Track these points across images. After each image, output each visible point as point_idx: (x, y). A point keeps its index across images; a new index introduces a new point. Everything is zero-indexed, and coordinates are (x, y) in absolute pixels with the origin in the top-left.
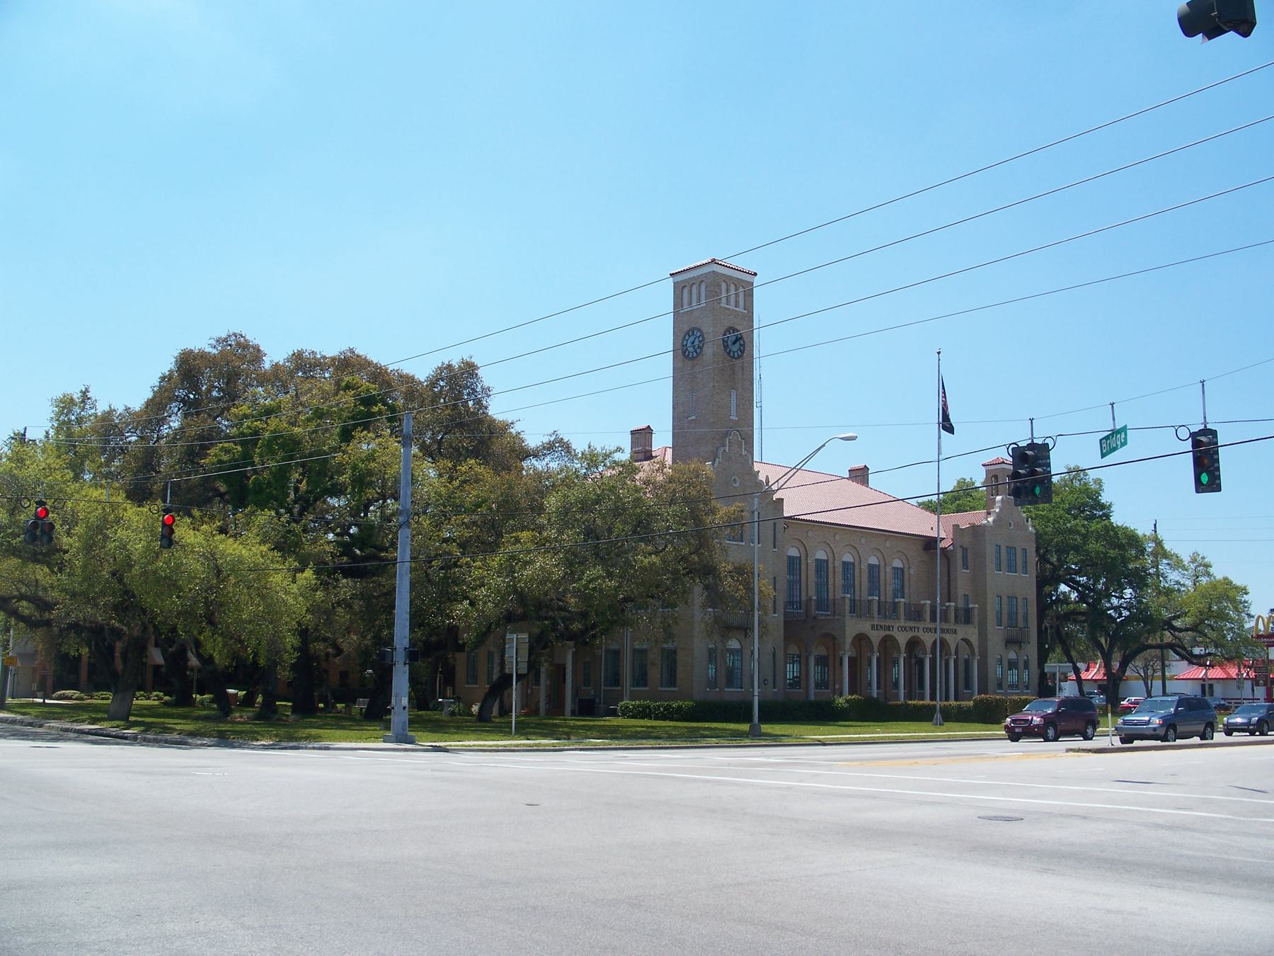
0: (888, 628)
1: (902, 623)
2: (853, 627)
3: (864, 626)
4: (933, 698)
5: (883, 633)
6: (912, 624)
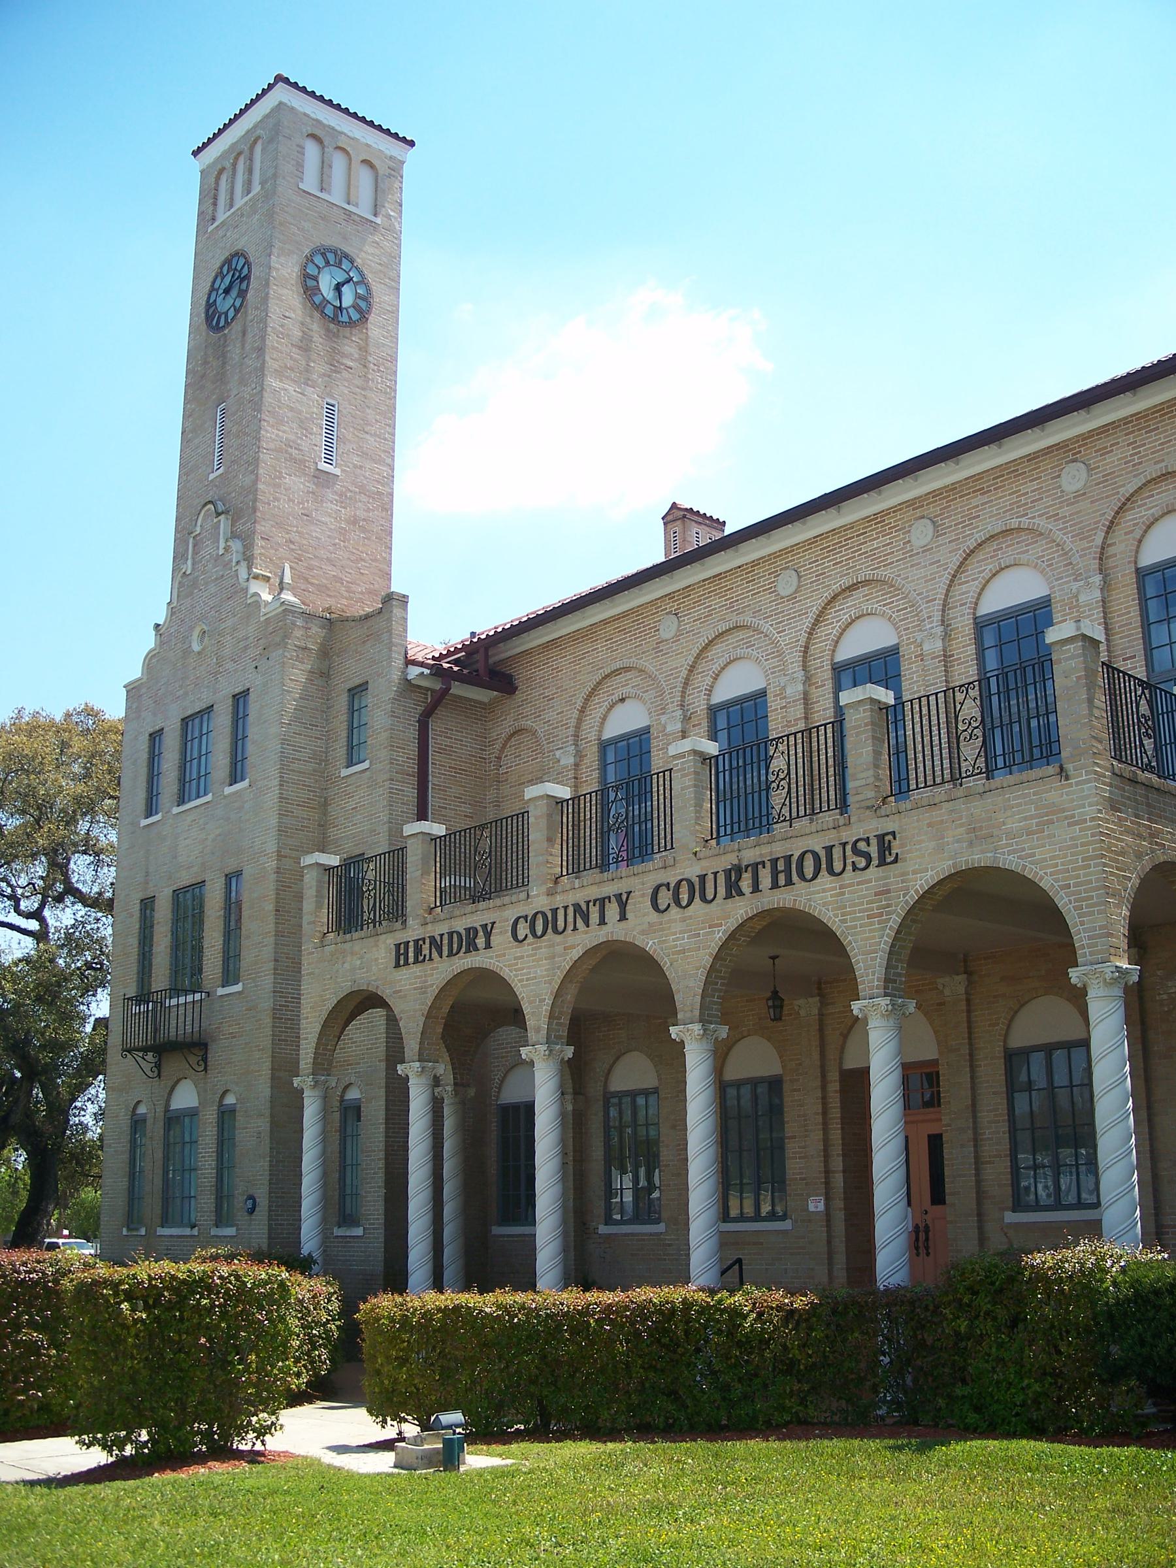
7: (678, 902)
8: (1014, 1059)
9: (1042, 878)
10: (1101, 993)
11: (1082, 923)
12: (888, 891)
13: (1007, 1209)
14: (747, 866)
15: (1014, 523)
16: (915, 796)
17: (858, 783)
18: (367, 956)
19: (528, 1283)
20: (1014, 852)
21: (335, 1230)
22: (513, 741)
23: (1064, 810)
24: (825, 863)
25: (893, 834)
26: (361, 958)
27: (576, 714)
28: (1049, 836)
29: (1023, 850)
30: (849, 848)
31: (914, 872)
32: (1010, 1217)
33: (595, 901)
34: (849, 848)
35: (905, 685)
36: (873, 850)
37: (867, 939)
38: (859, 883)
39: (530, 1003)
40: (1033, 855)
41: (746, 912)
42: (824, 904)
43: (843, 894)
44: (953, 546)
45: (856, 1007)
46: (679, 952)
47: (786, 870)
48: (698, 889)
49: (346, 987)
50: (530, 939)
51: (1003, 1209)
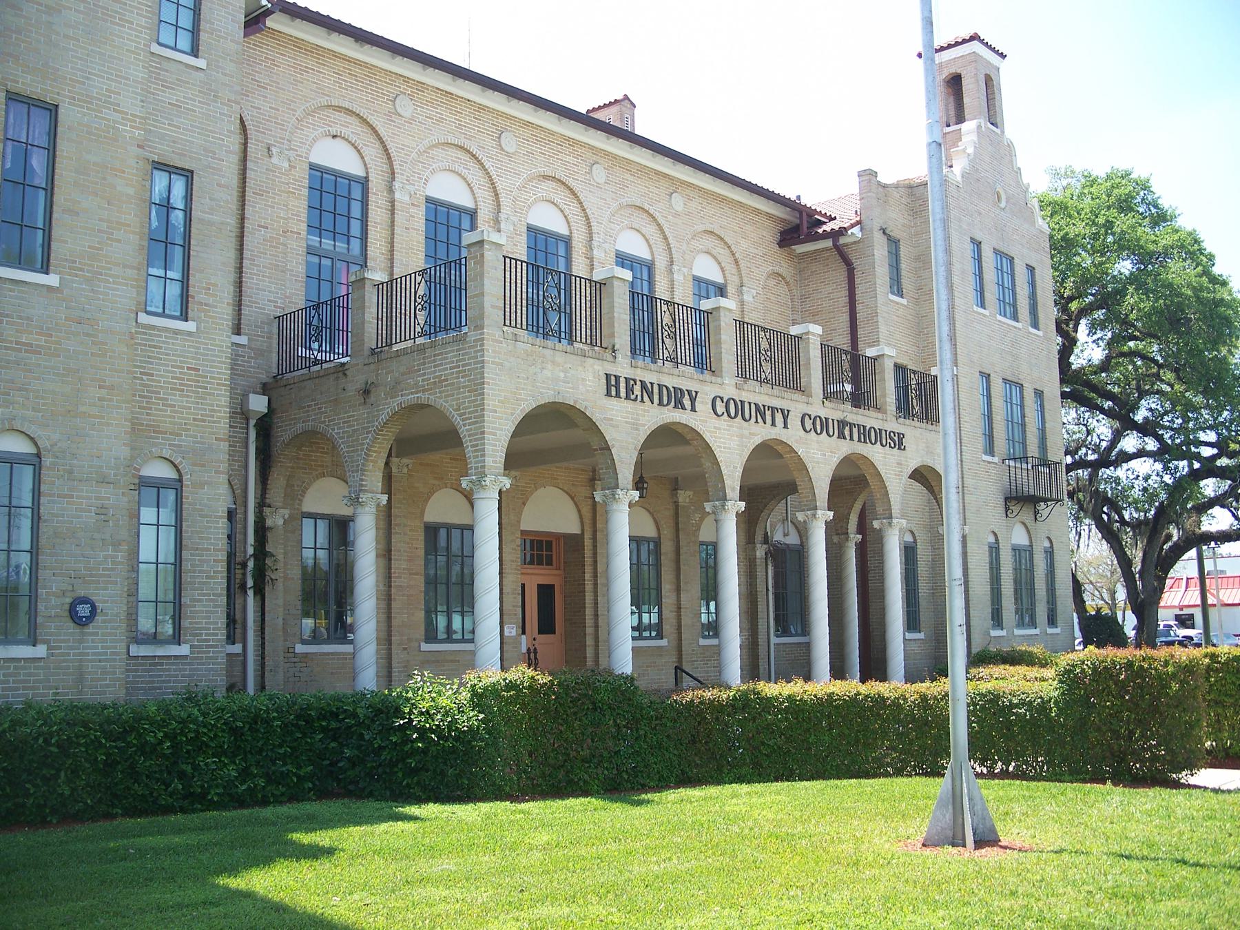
0: (677, 398)
1: (728, 386)
2: (513, 376)
3: (575, 377)
4: (838, 672)
5: (654, 416)
6: (756, 394)
8: (431, 531)
18: (572, 372)
19: (883, 678)
21: (423, 644)
26: (565, 371)
32: (425, 647)
49: (547, 397)
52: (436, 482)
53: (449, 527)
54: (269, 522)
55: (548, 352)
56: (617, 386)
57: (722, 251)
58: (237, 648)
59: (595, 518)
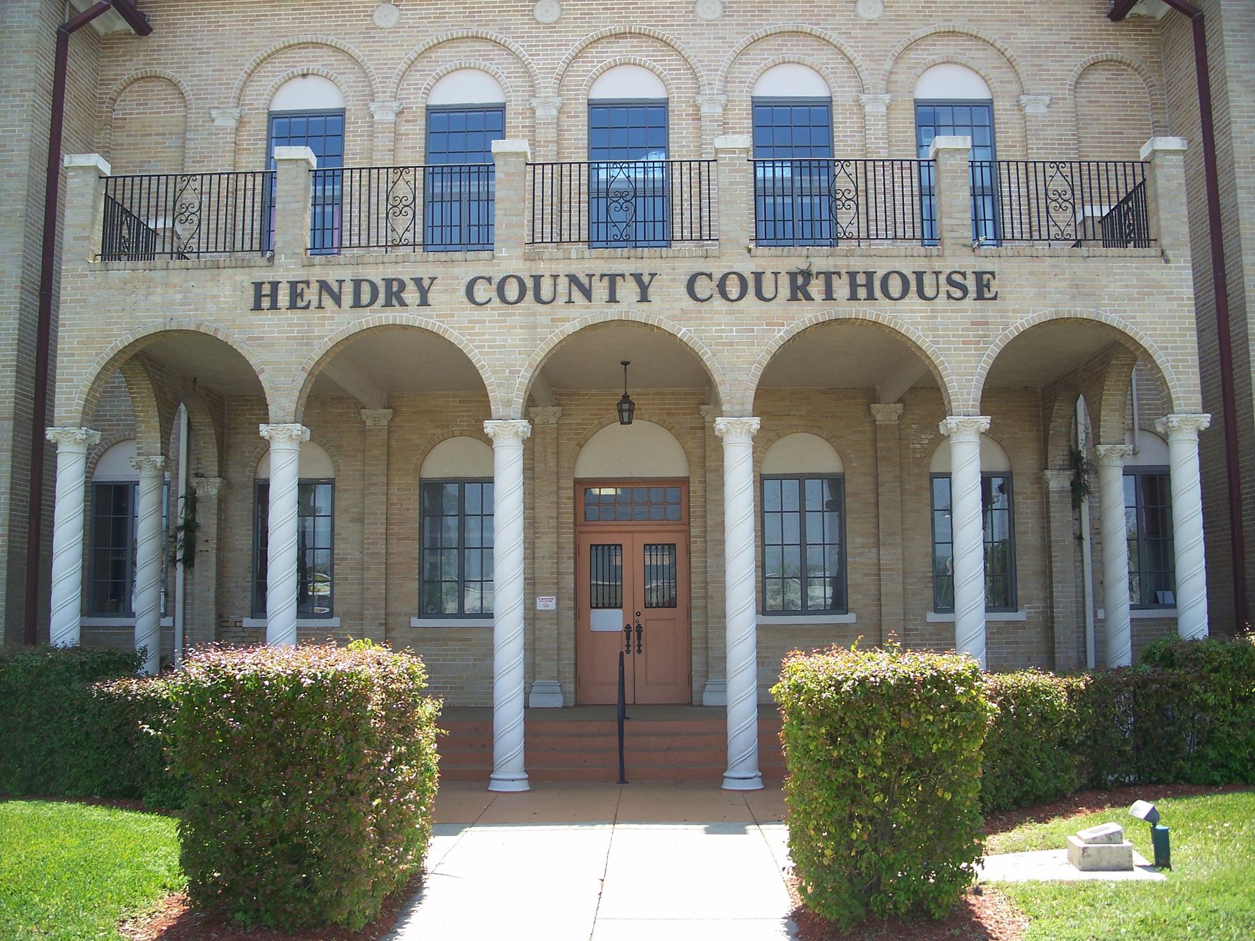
7: (724, 295)
8: (432, 489)
9: (1141, 338)
10: (70, 449)
11: (1179, 380)
12: (986, 323)
13: (414, 615)
14: (818, 273)
15: (807, 28)
16: (676, 246)
17: (952, 222)
20: (1116, 311)
22: (136, 86)
23: (1163, 287)
24: (915, 285)
25: (992, 274)
27: (243, 76)
28: (1149, 305)
29: (1125, 311)
30: (942, 278)
31: (1014, 311)
32: (416, 622)
33: (602, 276)
34: (942, 278)
35: (673, 148)
36: (971, 284)
37: (961, 362)
38: (953, 311)
39: (495, 372)
40: (1134, 317)
41: (816, 317)
42: (913, 324)
43: (936, 317)
44: (741, 29)
45: (264, 430)
46: (724, 344)
47: (865, 285)
48: (754, 285)
50: (496, 301)
51: (409, 615)
52: (438, 431)
53: (462, 482)
54: (200, 493)
55: (157, 275)
56: (274, 296)
57: (980, 54)
58: (167, 622)
59: (708, 454)
